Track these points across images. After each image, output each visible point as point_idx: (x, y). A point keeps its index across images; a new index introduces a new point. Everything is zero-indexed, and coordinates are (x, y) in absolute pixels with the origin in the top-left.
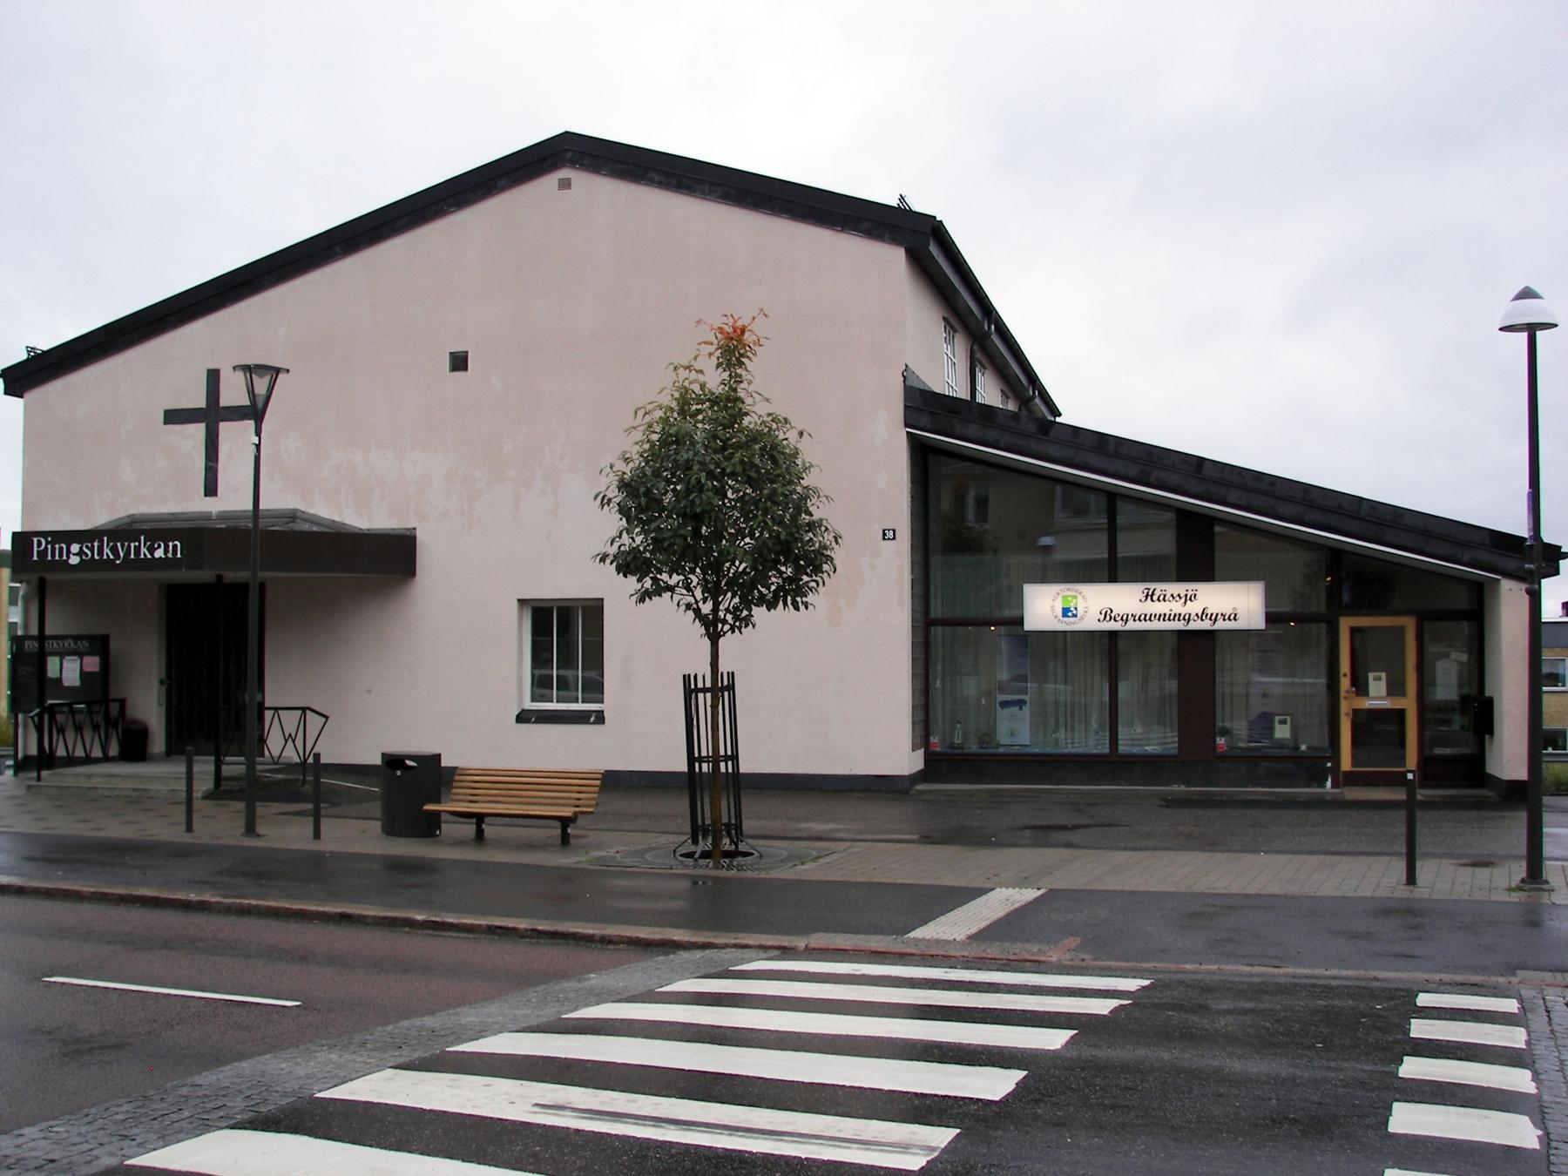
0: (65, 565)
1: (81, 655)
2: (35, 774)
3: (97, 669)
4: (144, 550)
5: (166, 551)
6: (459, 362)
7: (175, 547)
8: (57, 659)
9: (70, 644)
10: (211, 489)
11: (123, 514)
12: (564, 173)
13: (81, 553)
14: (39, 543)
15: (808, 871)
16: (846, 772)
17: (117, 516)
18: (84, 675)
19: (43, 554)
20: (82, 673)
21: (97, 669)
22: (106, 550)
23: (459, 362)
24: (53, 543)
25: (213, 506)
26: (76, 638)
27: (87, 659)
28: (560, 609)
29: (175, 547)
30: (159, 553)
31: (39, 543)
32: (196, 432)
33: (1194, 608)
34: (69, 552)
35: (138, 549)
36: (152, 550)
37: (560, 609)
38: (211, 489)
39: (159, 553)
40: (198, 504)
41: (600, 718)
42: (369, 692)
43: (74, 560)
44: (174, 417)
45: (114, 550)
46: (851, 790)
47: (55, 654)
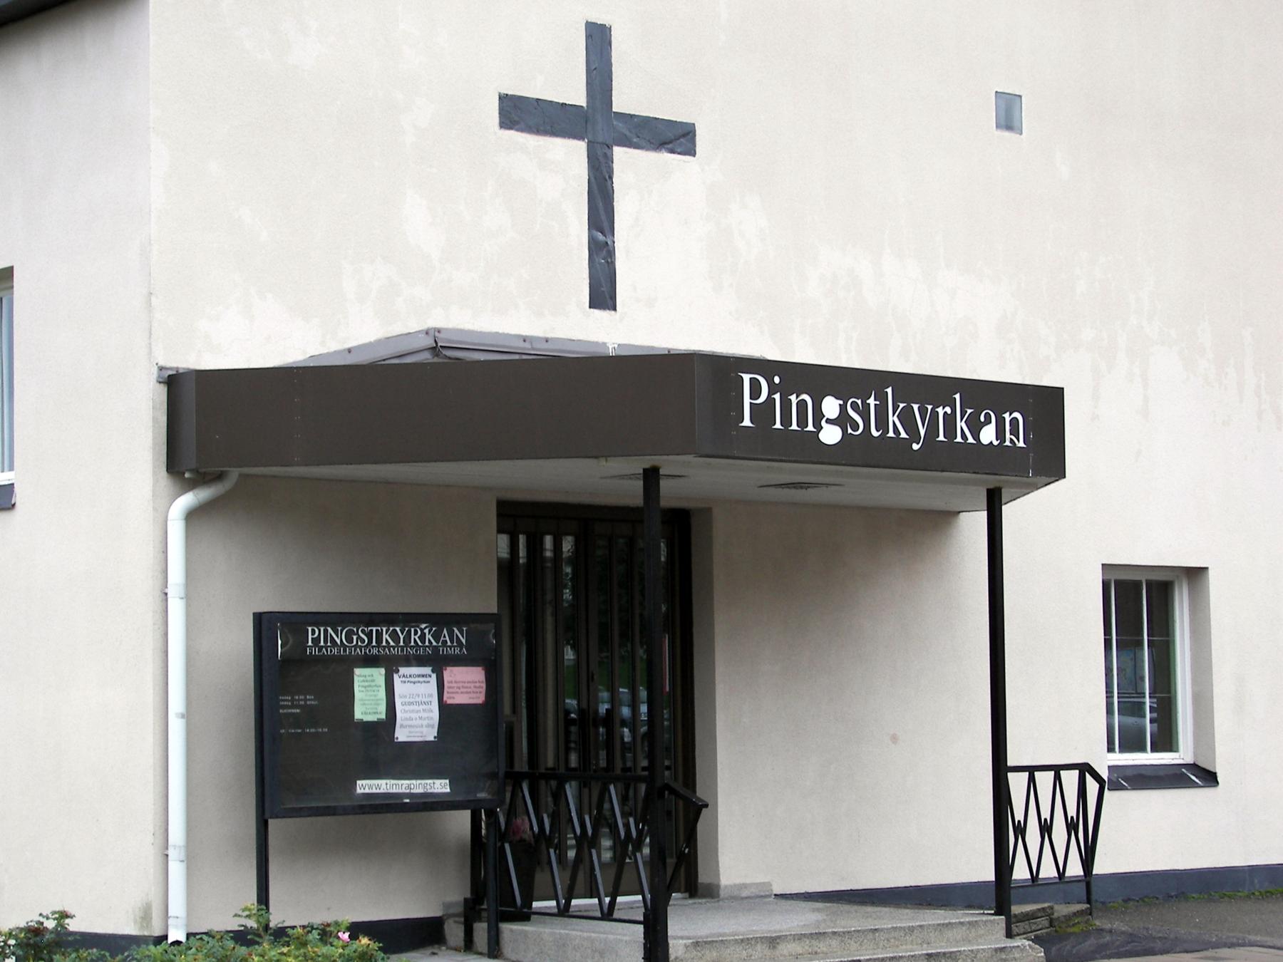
0: (808, 446)
1: (438, 662)
3: (479, 698)
5: (1000, 433)
6: (1008, 114)
7: (1014, 422)
8: (378, 674)
9: (423, 635)
10: (603, 295)
11: (414, 325)
13: (842, 420)
14: (755, 392)
16: (913, 884)
17: (397, 329)
19: (762, 413)
20: (446, 710)
21: (479, 698)
22: (893, 419)
23: (1008, 114)
26: (440, 621)
28: (1149, 584)
29: (1014, 422)
30: (988, 435)
31: (755, 392)
32: (570, 156)
34: (818, 415)
35: (950, 421)
36: (976, 428)
39: (988, 435)
42: (894, 739)
43: (831, 435)
45: (907, 418)
46: (1182, 896)
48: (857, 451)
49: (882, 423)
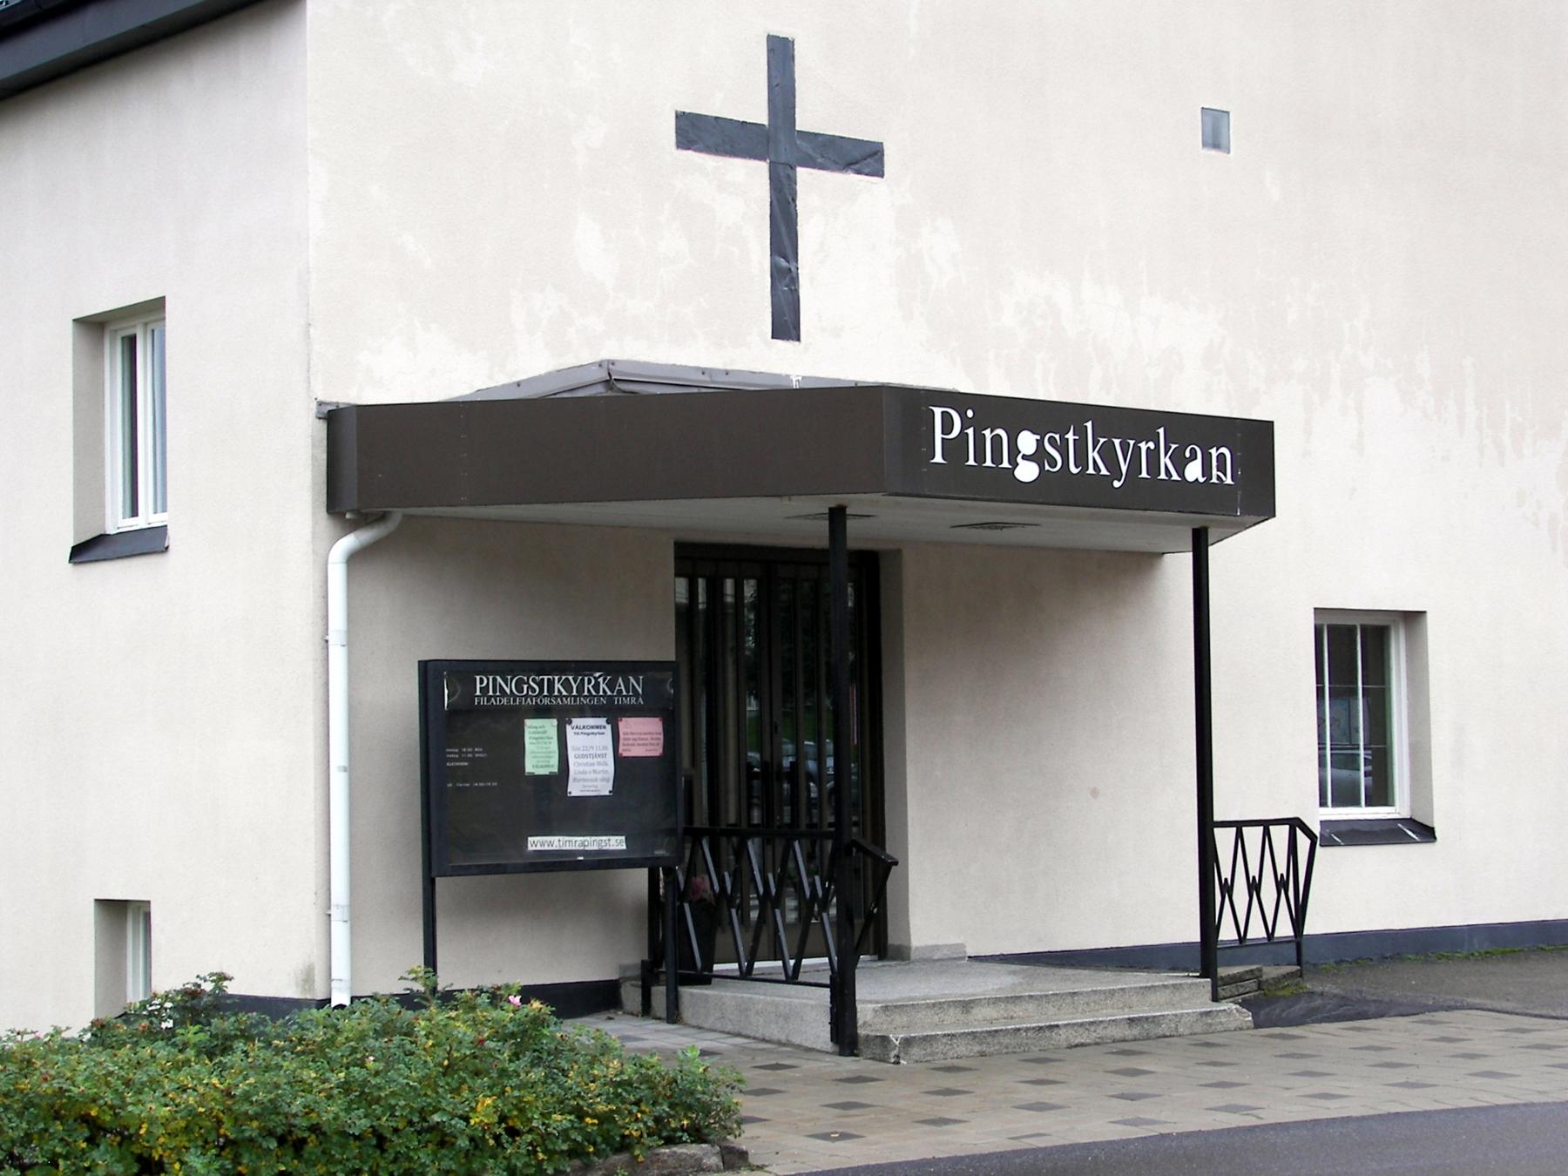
0: (1002, 485)
1: (612, 712)
3: (657, 751)
4: (1165, 460)
5: (1206, 470)
6: (1215, 131)
8: (550, 725)
11: (587, 357)
13: (1039, 456)
14: (947, 425)
17: (569, 361)
18: (625, 767)
19: (955, 448)
21: (657, 751)
22: (1093, 455)
23: (1215, 131)
24: (978, 425)
26: (615, 669)
27: (628, 725)
28: (1364, 629)
29: (1221, 457)
30: (1194, 471)
31: (947, 425)
34: (1014, 451)
35: (1153, 456)
36: (1180, 463)
37: (1364, 629)
38: (786, 325)
39: (1194, 471)
40: (756, 357)
41: (1427, 833)
42: (1095, 793)
43: (1027, 472)
44: (698, 132)
45: (1108, 454)
46: (1398, 957)
47: (542, 712)
48: (1056, 489)
49: (1081, 459)
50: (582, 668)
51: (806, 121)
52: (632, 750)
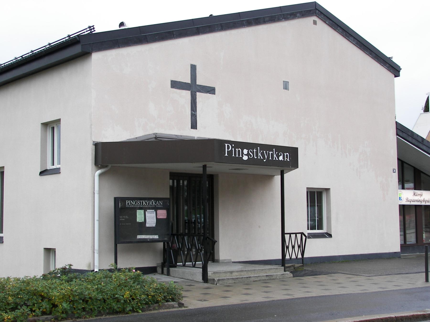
1: (156, 209)
2: (197, 273)
3: (165, 217)
6: (286, 86)
8: (142, 211)
10: (194, 126)
11: (151, 132)
12: (315, 18)
13: (248, 155)
14: (228, 148)
15: (51, 259)
19: (230, 153)
21: (165, 217)
23: (286, 86)
25: (196, 134)
27: (159, 211)
28: (317, 192)
30: (281, 158)
31: (228, 148)
33: (422, 198)
35: (272, 155)
36: (278, 156)
37: (317, 192)
38: (194, 126)
39: (281, 158)
40: (186, 132)
42: (259, 227)
44: (175, 85)
45: (263, 154)
46: (324, 262)
47: (140, 208)
48: (251, 161)
49: (257, 155)
50: (149, 199)
51: (199, 82)
52: (160, 217)
